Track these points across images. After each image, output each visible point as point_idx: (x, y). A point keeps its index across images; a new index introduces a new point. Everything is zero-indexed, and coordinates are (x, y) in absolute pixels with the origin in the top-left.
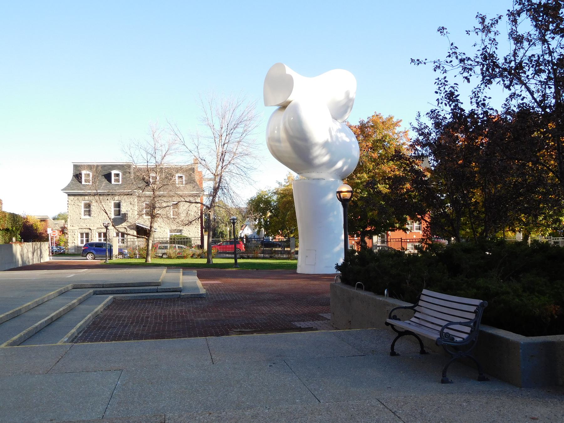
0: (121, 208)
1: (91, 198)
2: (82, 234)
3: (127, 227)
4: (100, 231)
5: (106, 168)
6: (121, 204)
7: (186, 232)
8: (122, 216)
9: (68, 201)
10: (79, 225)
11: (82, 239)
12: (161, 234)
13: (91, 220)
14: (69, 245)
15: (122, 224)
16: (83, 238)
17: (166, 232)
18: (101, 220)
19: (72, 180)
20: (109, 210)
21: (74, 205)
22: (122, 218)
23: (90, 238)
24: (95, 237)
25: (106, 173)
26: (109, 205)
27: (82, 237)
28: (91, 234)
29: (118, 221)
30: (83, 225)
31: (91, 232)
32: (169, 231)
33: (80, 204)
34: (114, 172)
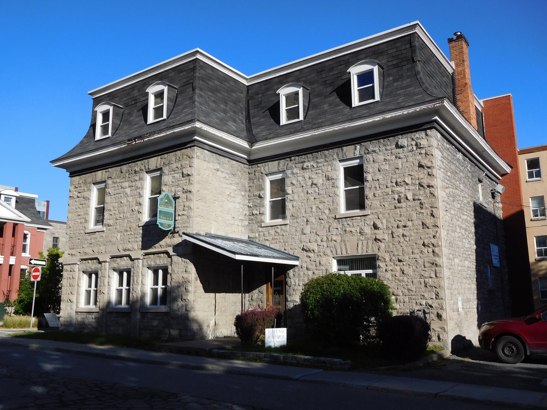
3: (170, 250)
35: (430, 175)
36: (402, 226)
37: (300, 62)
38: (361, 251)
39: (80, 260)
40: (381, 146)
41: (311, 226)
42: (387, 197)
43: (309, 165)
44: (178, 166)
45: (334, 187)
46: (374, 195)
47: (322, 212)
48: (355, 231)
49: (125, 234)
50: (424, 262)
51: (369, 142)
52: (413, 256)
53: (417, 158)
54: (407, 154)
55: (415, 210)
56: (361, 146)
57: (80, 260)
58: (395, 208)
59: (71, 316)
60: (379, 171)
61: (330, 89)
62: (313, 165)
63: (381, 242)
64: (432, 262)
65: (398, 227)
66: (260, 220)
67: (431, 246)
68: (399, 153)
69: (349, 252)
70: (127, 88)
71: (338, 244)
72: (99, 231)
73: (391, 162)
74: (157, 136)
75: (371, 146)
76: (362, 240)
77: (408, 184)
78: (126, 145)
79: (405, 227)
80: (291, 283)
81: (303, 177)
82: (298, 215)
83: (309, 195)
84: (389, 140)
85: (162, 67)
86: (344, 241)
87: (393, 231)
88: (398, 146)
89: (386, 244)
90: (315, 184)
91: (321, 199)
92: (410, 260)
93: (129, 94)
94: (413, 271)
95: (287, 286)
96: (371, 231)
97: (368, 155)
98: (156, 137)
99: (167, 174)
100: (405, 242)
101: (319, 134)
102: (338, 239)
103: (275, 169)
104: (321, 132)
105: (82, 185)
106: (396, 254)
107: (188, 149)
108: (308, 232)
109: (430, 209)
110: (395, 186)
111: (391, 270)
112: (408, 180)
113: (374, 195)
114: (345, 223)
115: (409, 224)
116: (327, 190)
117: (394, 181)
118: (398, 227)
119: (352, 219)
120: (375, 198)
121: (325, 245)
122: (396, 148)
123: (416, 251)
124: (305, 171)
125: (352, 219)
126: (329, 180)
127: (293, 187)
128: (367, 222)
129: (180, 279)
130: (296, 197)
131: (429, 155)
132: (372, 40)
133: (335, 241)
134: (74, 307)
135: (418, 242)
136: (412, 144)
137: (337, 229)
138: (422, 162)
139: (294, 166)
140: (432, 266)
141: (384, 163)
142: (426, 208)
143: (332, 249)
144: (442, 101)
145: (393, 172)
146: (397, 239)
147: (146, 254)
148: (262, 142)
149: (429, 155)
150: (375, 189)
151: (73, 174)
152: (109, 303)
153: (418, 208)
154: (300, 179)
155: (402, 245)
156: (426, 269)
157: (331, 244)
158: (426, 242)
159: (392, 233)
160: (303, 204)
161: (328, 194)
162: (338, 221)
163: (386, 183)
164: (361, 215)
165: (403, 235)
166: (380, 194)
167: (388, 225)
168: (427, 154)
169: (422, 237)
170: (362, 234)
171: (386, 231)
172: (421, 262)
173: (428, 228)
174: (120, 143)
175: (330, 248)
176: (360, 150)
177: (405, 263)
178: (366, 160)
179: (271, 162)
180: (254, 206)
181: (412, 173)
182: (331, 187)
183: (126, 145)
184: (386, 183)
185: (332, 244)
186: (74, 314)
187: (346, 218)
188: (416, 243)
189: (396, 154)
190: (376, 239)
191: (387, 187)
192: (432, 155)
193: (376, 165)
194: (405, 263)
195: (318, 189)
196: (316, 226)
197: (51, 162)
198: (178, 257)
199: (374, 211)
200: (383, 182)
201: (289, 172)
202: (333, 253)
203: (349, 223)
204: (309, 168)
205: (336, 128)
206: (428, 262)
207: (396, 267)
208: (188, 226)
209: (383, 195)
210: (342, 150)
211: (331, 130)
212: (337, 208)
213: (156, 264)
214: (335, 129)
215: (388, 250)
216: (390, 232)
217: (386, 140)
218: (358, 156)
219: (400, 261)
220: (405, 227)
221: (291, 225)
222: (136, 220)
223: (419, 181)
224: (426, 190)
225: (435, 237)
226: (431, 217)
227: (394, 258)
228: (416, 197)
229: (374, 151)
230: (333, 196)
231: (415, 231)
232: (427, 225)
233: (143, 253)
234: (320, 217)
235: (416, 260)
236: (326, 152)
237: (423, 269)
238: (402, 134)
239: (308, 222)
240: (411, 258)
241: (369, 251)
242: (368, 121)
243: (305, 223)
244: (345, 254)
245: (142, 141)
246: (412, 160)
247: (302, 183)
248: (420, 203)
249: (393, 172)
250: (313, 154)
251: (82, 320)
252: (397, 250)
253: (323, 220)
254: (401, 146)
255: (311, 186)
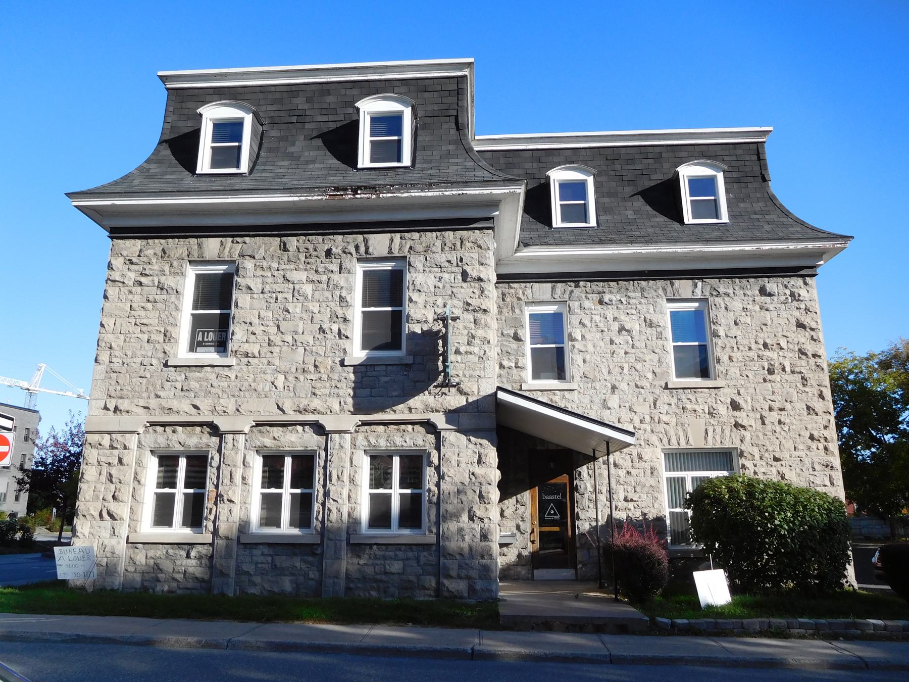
0: (406, 302)
1: (230, 247)
2: (168, 462)
3: (440, 421)
4: (270, 439)
5: (330, 99)
6: (408, 277)
7: (759, 463)
8: (409, 352)
9: (110, 267)
10: (153, 403)
11: (167, 490)
12: (622, 473)
13: (226, 372)
14: (78, 528)
15: (413, 402)
16: (280, 485)
17: (647, 466)
18: (281, 378)
19: (148, 161)
20: (334, 317)
21: (140, 284)
22: (410, 360)
23: (210, 486)
24: (238, 479)
25: (332, 126)
26: (336, 286)
27: (272, 476)
28: (215, 463)
29: (383, 379)
30: (174, 404)
31: (219, 451)
32: (661, 462)
33: (169, 281)
34: (687, 172)
35: (815, 340)
36: (777, 409)
37: (577, 136)
38: (712, 443)
39: (148, 425)
40: (737, 288)
41: (621, 397)
42: (752, 363)
43: (615, 299)
44: (450, 259)
45: (661, 338)
46: (730, 358)
47: (640, 376)
48: (701, 411)
49: (302, 378)
50: (813, 463)
51: (718, 280)
52: (797, 454)
53: (793, 313)
54: (779, 306)
55: (794, 387)
56: (704, 283)
57: (148, 425)
58: (765, 380)
59: (113, 553)
60: (736, 324)
61: (629, 190)
62: (620, 300)
63: (745, 430)
64: (825, 464)
65: (771, 409)
66: (519, 378)
67: (822, 440)
68: (766, 303)
69: (691, 441)
70: (273, 89)
71: (672, 429)
72: (216, 364)
73: (754, 313)
74: (417, 194)
75: (724, 286)
76: (713, 425)
77: (783, 349)
78: (324, 198)
79: (782, 410)
80: (586, 488)
81: (602, 316)
82: (595, 376)
83: (614, 346)
84: (748, 281)
85: (378, 71)
86: (682, 424)
87: (764, 414)
88: (763, 292)
89: (752, 433)
90: (628, 331)
91: (637, 355)
92: (792, 458)
93: (280, 101)
94: (797, 476)
95: (576, 494)
96: (728, 412)
97: (716, 299)
98: (413, 194)
99: (422, 271)
100: (783, 433)
101: (647, 253)
102: (673, 421)
103: (547, 297)
104: (652, 251)
105: (154, 261)
106: (770, 449)
107: (476, 231)
108: (616, 406)
109: (818, 388)
110: (763, 349)
111: (764, 473)
112: (783, 344)
113: (729, 359)
114: (683, 397)
115: (788, 406)
116: (648, 342)
117: (761, 342)
118: (771, 409)
119: (695, 392)
120: (732, 364)
121: (649, 428)
122: (761, 295)
123: (801, 447)
124: (605, 307)
125: (695, 392)
126: (651, 327)
127: (583, 330)
128: (720, 398)
129: (465, 477)
130: (590, 348)
131: (811, 312)
132: (702, 135)
133: (665, 424)
134: (124, 531)
135: (802, 433)
136: (785, 294)
137: (670, 405)
138: (803, 320)
139: (583, 296)
140: (825, 469)
141: (744, 314)
142: (812, 386)
143: (661, 435)
144: (846, 241)
145: (757, 328)
146: (769, 427)
147: (364, 424)
148: (538, 247)
149: (811, 312)
150: (730, 350)
151: (117, 233)
152: (244, 526)
153: (800, 386)
154: (597, 318)
155: (779, 437)
156: (816, 473)
157: (658, 428)
158: (816, 434)
159: (762, 418)
160: (604, 360)
161: (651, 348)
162: (671, 393)
163: (748, 343)
164: (711, 386)
165: (780, 422)
166: (741, 359)
167: (754, 405)
168: (809, 310)
169: (808, 426)
170: (712, 416)
171: (751, 415)
172: (807, 463)
173: (817, 414)
174: (310, 190)
175: (658, 434)
176: (702, 289)
177: (783, 463)
178: (713, 306)
179: (537, 284)
180: (504, 352)
181: (788, 334)
182: (655, 339)
183: (324, 198)
184: (748, 343)
185: (661, 428)
186: (121, 548)
187: (541, 391)
188: (799, 435)
189: (760, 304)
190: (737, 425)
191: (750, 349)
192: (816, 313)
193: (731, 315)
194: (783, 463)
195: (632, 338)
196: (630, 396)
197: (69, 195)
198: (458, 434)
199: (732, 383)
200: (744, 341)
201: (576, 306)
202: (663, 442)
203: (690, 396)
204: (614, 303)
205: (749, 247)
206: (819, 463)
207: (771, 469)
208: (482, 376)
209: (743, 360)
210: (672, 285)
211: (671, 250)
212: (668, 371)
213: (392, 445)
214: (677, 250)
215: (757, 442)
216: (758, 416)
217: (744, 281)
218: (699, 297)
219: (776, 459)
220: (782, 410)
221: (581, 391)
222: (333, 351)
223: (800, 347)
224: (810, 360)
225: (827, 428)
226: (820, 399)
227: (767, 455)
228: (797, 369)
229: (727, 294)
230: (660, 352)
231: (797, 417)
232: (816, 410)
233: (147, 422)
234: (638, 383)
235: (801, 460)
236: (643, 283)
237: (812, 473)
238: (768, 277)
239: (616, 390)
240: (793, 456)
241: (725, 443)
242: (734, 248)
243: (610, 391)
244: (683, 445)
245: (374, 196)
246: (786, 316)
247: (601, 325)
248: (803, 378)
249: (757, 328)
250: (620, 282)
251: (152, 562)
252: (772, 444)
253: (643, 388)
254: (770, 293)
255: (618, 332)
